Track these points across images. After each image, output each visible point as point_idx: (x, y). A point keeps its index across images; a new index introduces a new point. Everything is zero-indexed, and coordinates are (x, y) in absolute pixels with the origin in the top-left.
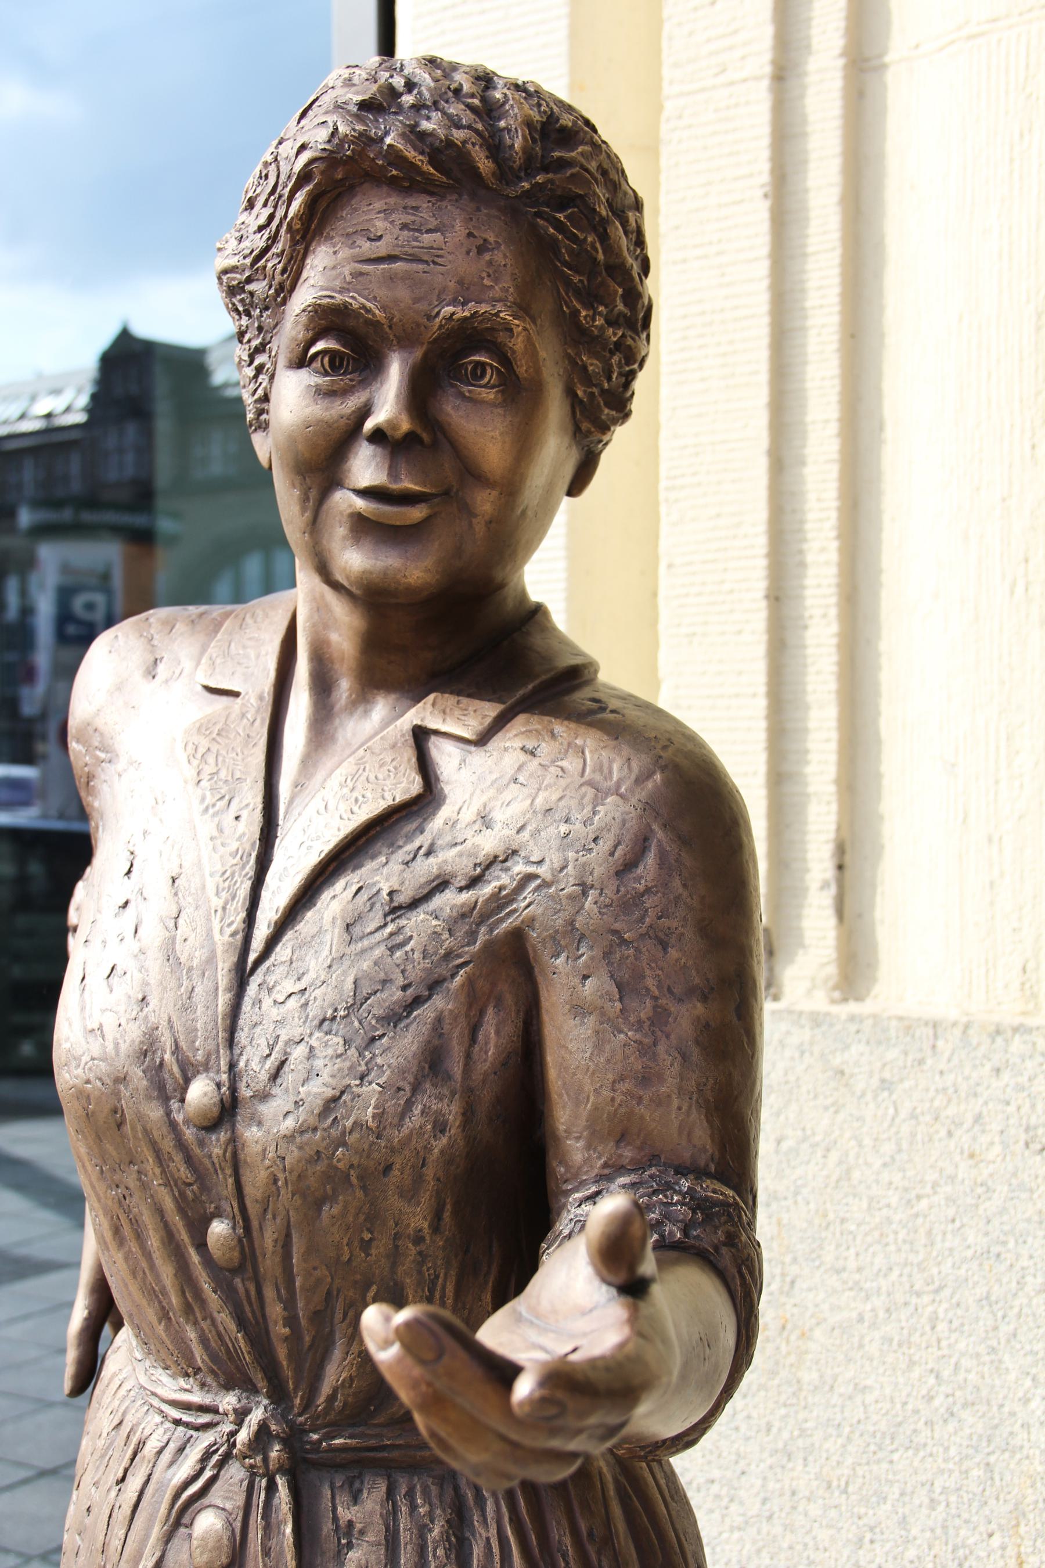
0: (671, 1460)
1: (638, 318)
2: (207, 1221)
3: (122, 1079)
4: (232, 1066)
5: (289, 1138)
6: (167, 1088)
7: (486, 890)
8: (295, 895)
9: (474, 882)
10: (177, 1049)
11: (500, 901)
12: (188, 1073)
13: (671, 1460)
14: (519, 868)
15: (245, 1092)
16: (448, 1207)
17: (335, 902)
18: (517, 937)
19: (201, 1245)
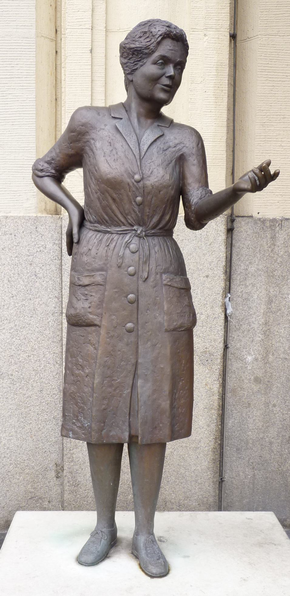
1: (188, 47)
7: (178, 148)
10: (131, 171)
11: (180, 150)
15: (145, 176)
17: (154, 149)
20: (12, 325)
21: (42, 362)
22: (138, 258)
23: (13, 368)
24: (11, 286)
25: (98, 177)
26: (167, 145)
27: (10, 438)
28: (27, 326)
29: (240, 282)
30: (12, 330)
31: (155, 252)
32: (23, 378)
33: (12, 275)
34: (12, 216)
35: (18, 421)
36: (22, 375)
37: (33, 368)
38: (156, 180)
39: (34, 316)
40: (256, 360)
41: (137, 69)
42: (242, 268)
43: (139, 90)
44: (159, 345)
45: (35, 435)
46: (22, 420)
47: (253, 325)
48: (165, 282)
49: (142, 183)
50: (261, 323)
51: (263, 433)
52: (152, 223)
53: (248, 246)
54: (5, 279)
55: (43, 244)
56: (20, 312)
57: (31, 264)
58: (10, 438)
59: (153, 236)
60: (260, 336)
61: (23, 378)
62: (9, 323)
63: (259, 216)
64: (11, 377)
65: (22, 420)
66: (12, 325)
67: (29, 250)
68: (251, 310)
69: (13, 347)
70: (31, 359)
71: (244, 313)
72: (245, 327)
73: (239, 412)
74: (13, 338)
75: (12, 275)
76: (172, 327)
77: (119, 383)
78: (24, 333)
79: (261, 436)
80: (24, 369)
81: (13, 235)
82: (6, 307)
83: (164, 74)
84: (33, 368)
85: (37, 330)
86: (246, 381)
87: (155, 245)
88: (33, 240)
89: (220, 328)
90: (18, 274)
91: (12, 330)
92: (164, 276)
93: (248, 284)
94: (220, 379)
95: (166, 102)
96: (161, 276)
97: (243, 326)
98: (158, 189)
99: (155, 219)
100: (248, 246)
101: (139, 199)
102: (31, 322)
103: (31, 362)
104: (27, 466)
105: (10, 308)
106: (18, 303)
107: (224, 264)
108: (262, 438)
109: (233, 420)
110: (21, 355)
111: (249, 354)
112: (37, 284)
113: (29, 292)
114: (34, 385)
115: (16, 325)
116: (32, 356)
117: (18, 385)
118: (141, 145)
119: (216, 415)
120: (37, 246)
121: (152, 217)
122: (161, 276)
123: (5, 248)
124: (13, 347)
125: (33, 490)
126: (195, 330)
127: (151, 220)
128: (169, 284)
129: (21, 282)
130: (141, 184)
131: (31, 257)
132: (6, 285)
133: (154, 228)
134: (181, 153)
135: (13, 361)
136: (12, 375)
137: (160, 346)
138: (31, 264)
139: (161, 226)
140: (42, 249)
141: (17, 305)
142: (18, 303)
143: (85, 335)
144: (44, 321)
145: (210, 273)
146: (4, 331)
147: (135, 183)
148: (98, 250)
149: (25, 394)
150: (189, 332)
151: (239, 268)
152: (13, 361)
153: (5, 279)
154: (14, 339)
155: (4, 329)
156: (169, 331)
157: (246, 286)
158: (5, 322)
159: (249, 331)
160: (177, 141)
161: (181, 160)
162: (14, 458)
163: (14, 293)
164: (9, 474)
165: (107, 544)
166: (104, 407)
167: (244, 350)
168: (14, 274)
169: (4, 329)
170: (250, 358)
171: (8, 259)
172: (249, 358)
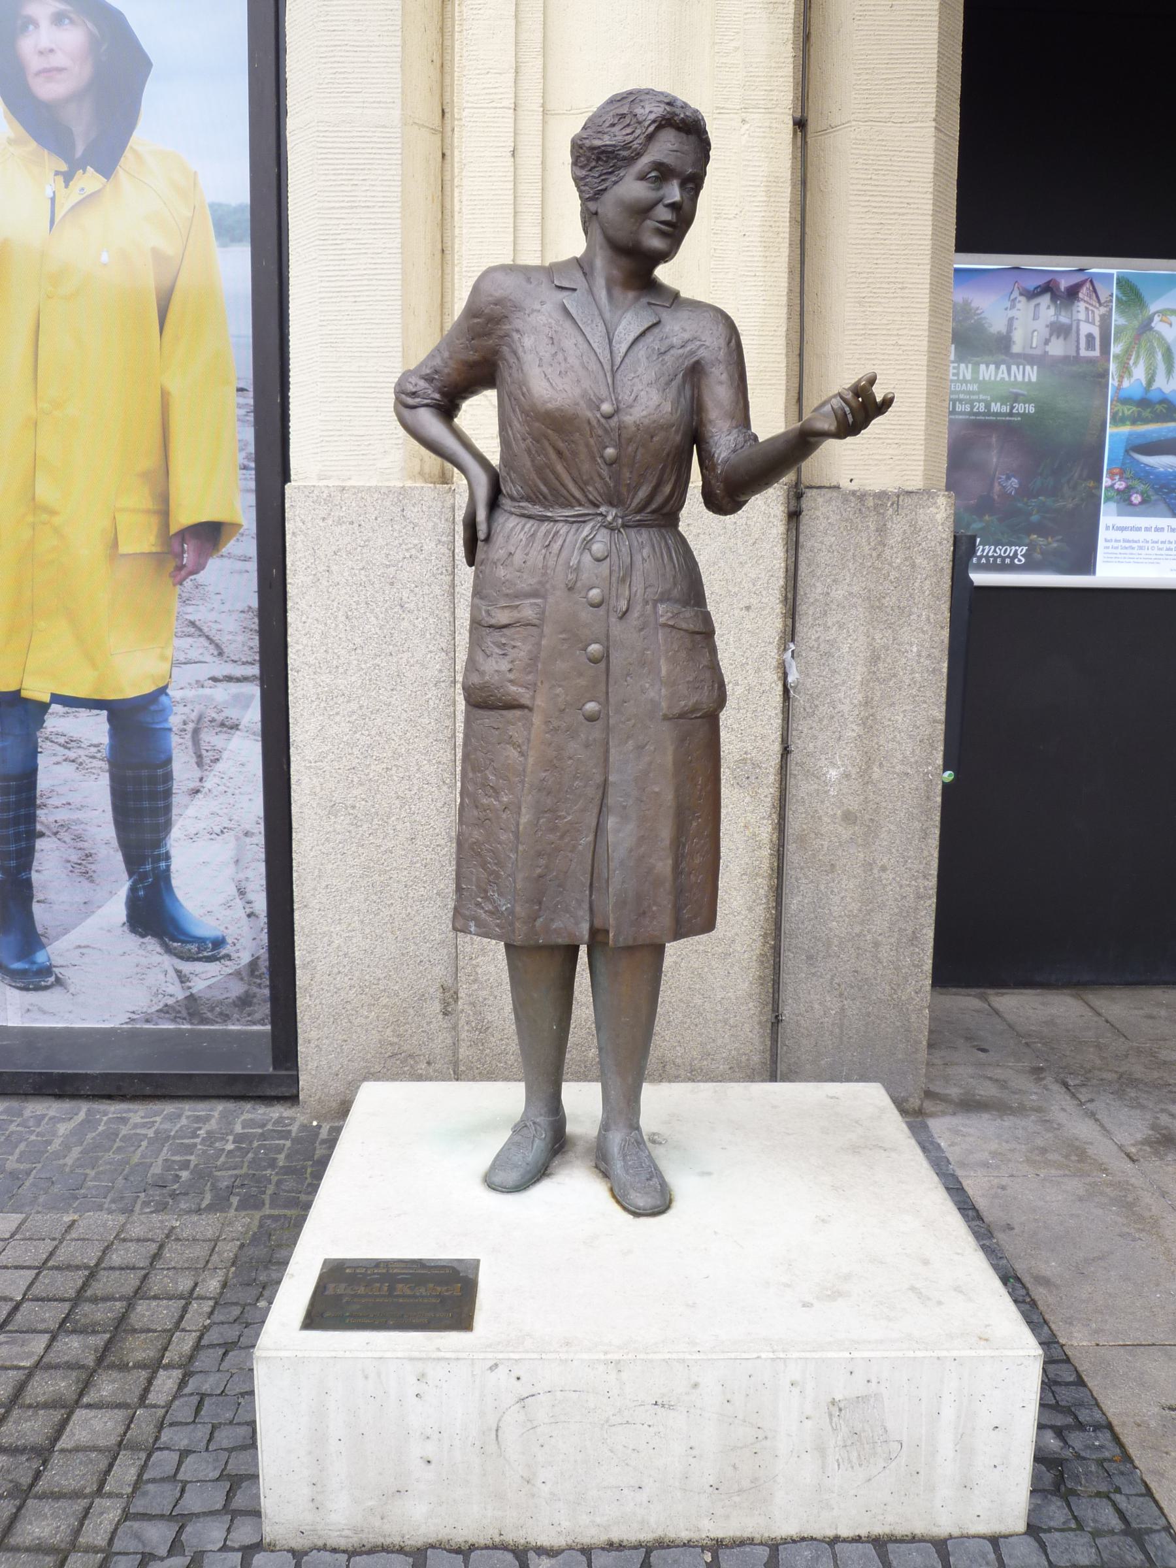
1: (709, 144)
11: (692, 353)
15: (622, 406)
17: (641, 351)
20: (354, 706)
23: (355, 792)
24: (353, 627)
25: (527, 408)
26: (667, 343)
28: (384, 707)
32: (377, 813)
35: (366, 900)
36: (373, 806)
40: (847, 776)
41: (605, 190)
42: (819, 590)
43: (611, 232)
45: (399, 929)
46: (374, 898)
47: (840, 707)
48: (662, 620)
55: (416, 542)
56: (370, 680)
57: (392, 584)
60: (855, 727)
61: (377, 813)
62: (348, 702)
63: (853, 486)
66: (354, 706)
72: (823, 710)
73: (812, 882)
74: (355, 732)
76: (676, 711)
79: (857, 930)
80: (379, 796)
81: (356, 525)
82: (341, 670)
85: (404, 715)
88: (396, 534)
92: (661, 608)
93: (830, 624)
96: (655, 607)
97: (821, 708)
99: (642, 493)
102: (393, 700)
104: (384, 990)
105: (349, 673)
106: (366, 662)
108: (858, 935)
109: (799, 898)
111: (833, 764)
112: (405, 624)
115: (361, 707)
116: (394, 769)
117: (365, 827)
122: (655, 607)
123: (339, 550)
125: (396, 1040)
126: (723, 716)
127: (636, 494)
130: (614, 422)
133: (640, 510)
135: (356, 780)
136: (354, 807)
138: (392, 584)
139: (654, 506)
140: (413, 552)
142: (366, 662)
145: (754, 601)
146: (338, 718)
147: (603, 420)
148: (527, 554)
150: (711, 720)
152: (356, 780)
153: (340, 614)
154: (358, 736)
155: (337, 714)
158: (340, 700)
161: (695, 372)
163: (358, 641)
166: (539, 871)
167: (823, 757)
168: (358, 603)
169: (337, 714)
170: (834, 773)
172: (833, 774)
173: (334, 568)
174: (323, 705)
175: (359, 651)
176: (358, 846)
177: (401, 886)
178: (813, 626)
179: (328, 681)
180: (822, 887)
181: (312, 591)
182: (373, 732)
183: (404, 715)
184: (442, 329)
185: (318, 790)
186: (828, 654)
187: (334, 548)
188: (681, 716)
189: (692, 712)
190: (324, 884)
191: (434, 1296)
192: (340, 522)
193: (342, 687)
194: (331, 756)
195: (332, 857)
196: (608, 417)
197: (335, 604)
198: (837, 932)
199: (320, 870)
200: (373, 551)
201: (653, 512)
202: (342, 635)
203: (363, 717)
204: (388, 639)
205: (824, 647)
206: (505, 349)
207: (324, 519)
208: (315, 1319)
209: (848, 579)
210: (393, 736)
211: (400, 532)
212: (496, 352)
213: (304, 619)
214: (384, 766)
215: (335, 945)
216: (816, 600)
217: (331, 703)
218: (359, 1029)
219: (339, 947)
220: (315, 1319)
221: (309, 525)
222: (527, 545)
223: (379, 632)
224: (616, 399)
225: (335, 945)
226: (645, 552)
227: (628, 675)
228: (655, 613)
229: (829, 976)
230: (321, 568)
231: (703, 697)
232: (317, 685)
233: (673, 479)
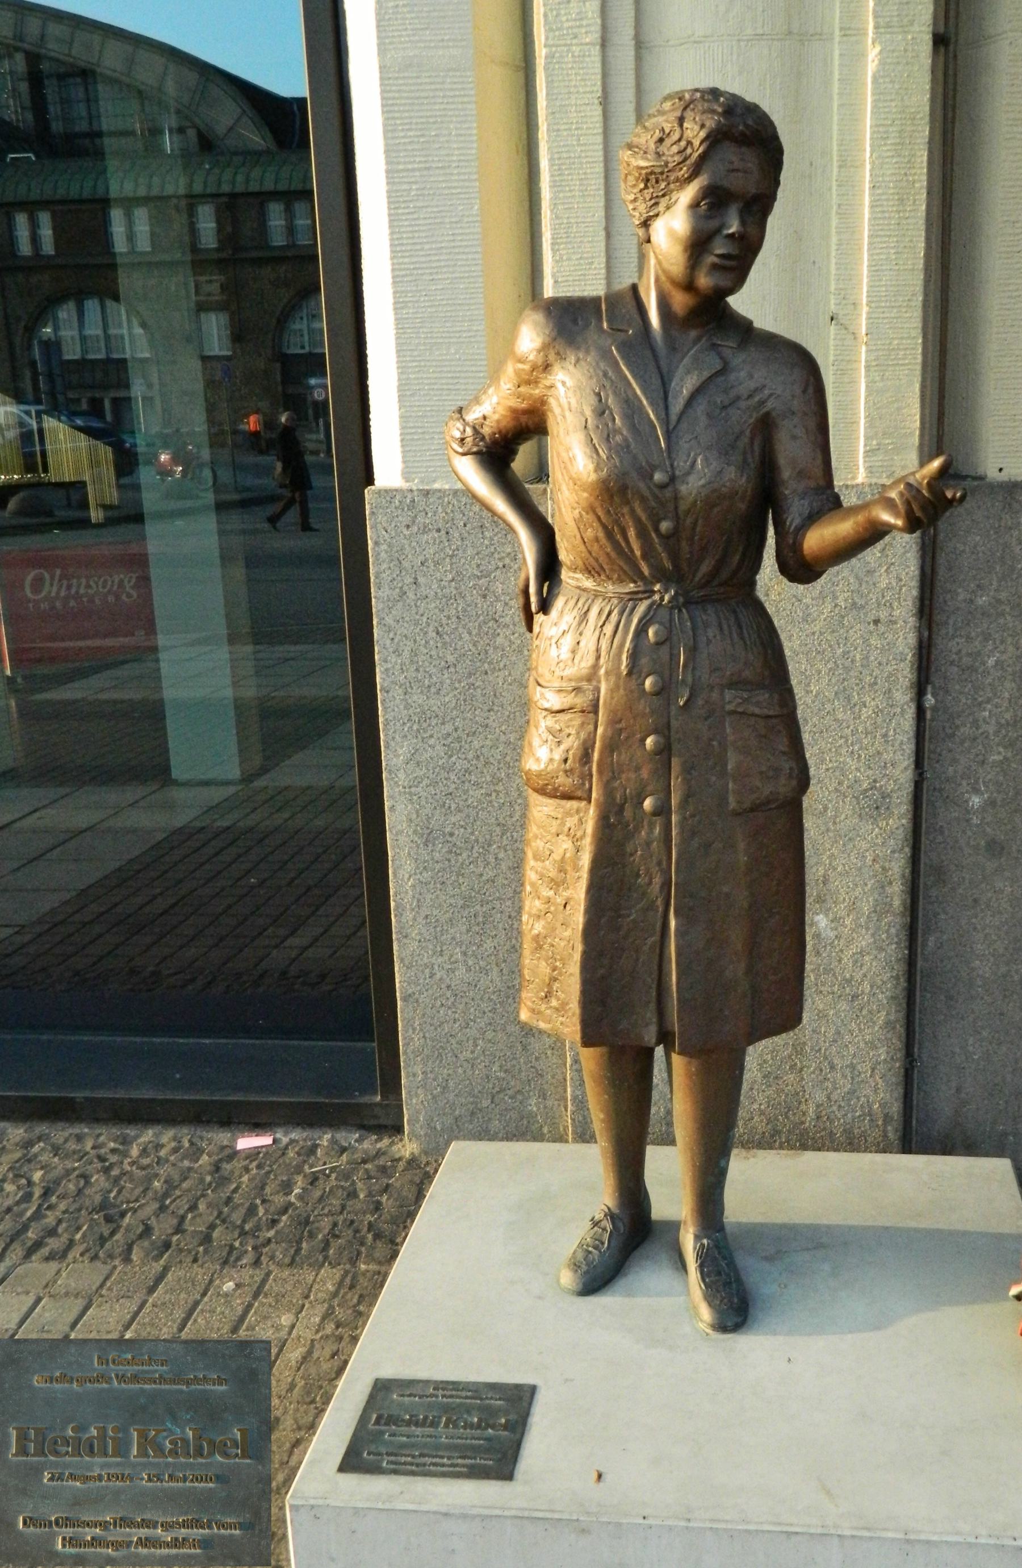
0: (546, 296)
1: (780, 151)
2: (659, 521)
3: (625, 474)
4: (672, 466)
5: (703, 486)
6: (647, 475)
7: (756, 399)
8: (345, 34)
9: (750, 396)
10: (647, 462)
11: (762, 403)
12: (653, 468)
13: (546, 296)
14: (766, 392)
15: (677, 473)
16: (70, 665)
17: (701, 408)
18: (767, 414)
19: (657, 530)
20: (449, 728)
21: (517, 808)
22: (668, 657)
23: (453, 819)
24: (445, 644)
25: (574, 476)
26: (733, 394)
27: (453, 966)
28: (481, 729)
29: (956, 630)
30: (450, 740)
31: (708, 639)
32: (477, 841)
33: (444, 621)
34: (440, 491)
35: (468, 931)
36: (472, 833)
37: (497, 819)
38: (702, 482)
39: (496, 708)
40: (992, 803)
41: (657, 215)
42: (961, 597)
43: (666, 265)
44: (718, 845)
45: (505, 961)
46: (477, 929)
47: (984, 727)
48: (729, 707)
49: (670, 489)
50: (1003, 721)
51: (1007, 964)
52: (699, 575)
53: (975, 547)
54: (431, 628)
55: (509, 550)
56: (465, 700)
57: (484, 596)
58: (453, 966)
59: (703, 601)
60: (1001, 749)
61: (477, 841)
62: (443, 724)
63: (1003, 477)
64: (450, 839)
65: (477, 929)
66: (449, 728)
67: (478, 566)
68: (981, 693)
69: (453, 777)
70: (491, 802)
71: (964, 701)
72: (966, 730)
73: (952, 917)
74: (451, 756)
75: (444, 621)
76: (747, 805)
77: (634, 921)
78: (476, 744)
79: (1003, 969)
80: (478, 823)
81: (443, 532)
82: (433, 690)
83: (718, 231)
84: (497, 819)
85: (503, 738)
86: (967, 851)
87: (706, 625)
88: (486, 542)
89: (906, 736)
90: (458, 617)
91: (450, 740)
92: (728, 695)
93: (973, 634)
94: (907, 850)
95: (732, 291)
96: (722, 694)
97: (962, 730)
98: (713, 499)
99: (705, 568)
100: (975, 547)
101: (665, 526)
102: (490, 722)
103: (493, 806)
104: (490, 1024)
105: (442, 693)
106: (460, 682)
107: (915, 593)
108: (1004, 976)
109: (938, 934)
110: (471, 793)
111: (976, 791)
112: (499, 640)
113: (482, 656)
114: (501, 855)
115: (456, 730)
116: (494, 794)
117: (464, 855)
118: (670, 399)
119: (898, 927)
120: (496, 556)
121: (700, 561)
122: (722, 694)
123: (426, 560)
124: (453, 777)
125: (502, 1075)
126: (806, 801)
127: (697, 570)
128: (740, 710)
129: (466, 636)
130: (668, 493)
131: (483, 581)
132: (431, 642)
133: (707, 583)
134: (765, 410)
135: (453, 806)
136: (451, 835)
137: (721, 845)
138: (484, 596)
139: (725, 574)
140: (507, 561)
141: (457, 685)
142: (460, 682)
143: (559, 816)
144: (518, 719)
145: (883, 615)
146: (432, 741)
147: (656, 491)
148: (581, 634)
149: (481, 875)
150: (791, 811)
151: (957, 596)
152: (453, 806)
153: (431, 628)
154: (453, 759)
155: (431, 736)
156: (739, 814)
157: (969, 639)
158: (434, 722)
159: (975, 739)
160: (752, 385)
161: (766, 426)
162: (461, 1007)
163: (450, 658)
164: (453, 1041)
165: (630, 1238)
166: (601, 972)
167: (964, 783)
168: (449, 618)
169: (431, 736)
170: (977, 800)
171: (435, 586)
172: (976, 801)
173: (421, 580)
174: (415, 727)
175: (452, 669)
176: (458, 876)
177: (505, 918)
178: (953, 637)
179: (420, 701)
180: (963, 922)
181: (400, 604)
182: (470, 756)
183: (503, 738)
184: (191, 822)
185: (414, 816)
186: (972, 669)
187: (421, 558)
188: (753, 809)
189: (769, 802)
190: (423, 915)
191: (477, 1430)
192: (425, 530)
193: (435, 708)
194: (426, 782)
195: (432, 886)
196: (663, 487)
197: (425, 620)
198: (981, 972)
199: (419, 901)
200: (463, 561)
201: (720, 585)
202: (433, 653)
203: (459, 739)
204: (482, 656)
205: (966, 661)
206: (552, 401)
207: (408, 527)
208: (354, 1461)
209: (995, 583)
210: (491, 760)
211: (492, 539)
212: (543, 402)
213: (391, 635)
214: (483, 791)
215: (438, 976)
216: (958, 609)
217: (425, 725)
218: (465, 1064)
219: (441, 979)
220: (354, 1461)
221: (393, 534)
222: (580, 624)
223: (473, 649)
224: (672, 466)
225: (438, 976)
226: (710, 633)
227: (692, 768)
228: (723, 698)
229: (971, 1019)
230: (409, 580)
231: (784, 787)
232: (408, 706)
233: (741, 549)
